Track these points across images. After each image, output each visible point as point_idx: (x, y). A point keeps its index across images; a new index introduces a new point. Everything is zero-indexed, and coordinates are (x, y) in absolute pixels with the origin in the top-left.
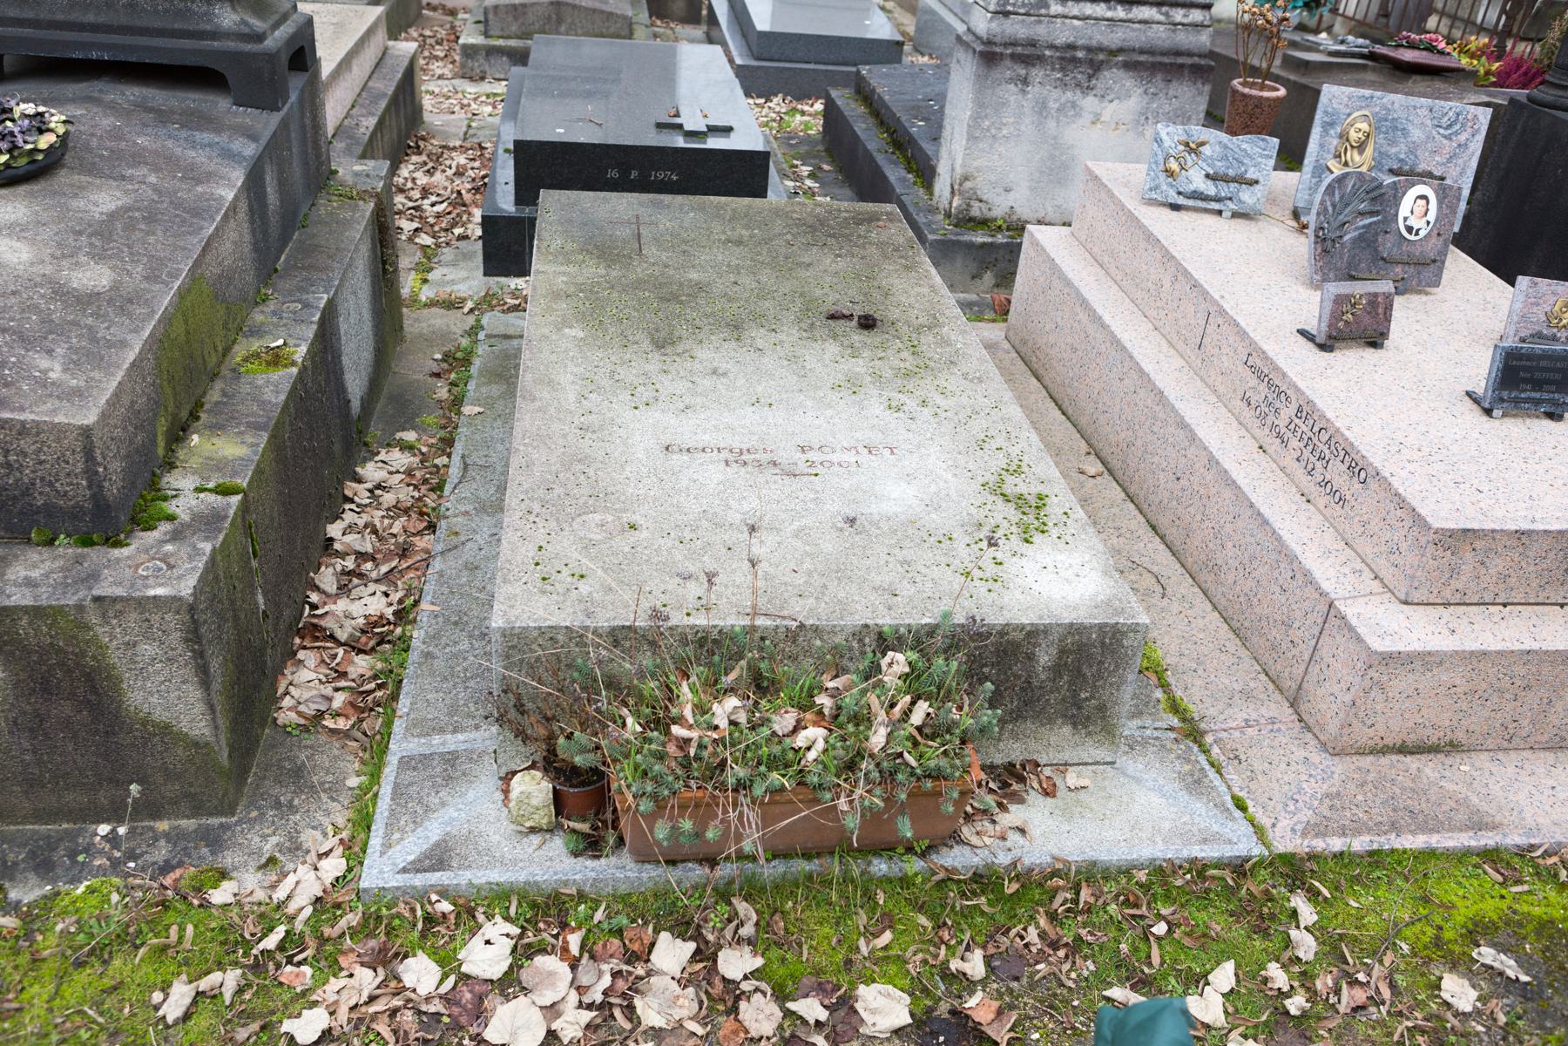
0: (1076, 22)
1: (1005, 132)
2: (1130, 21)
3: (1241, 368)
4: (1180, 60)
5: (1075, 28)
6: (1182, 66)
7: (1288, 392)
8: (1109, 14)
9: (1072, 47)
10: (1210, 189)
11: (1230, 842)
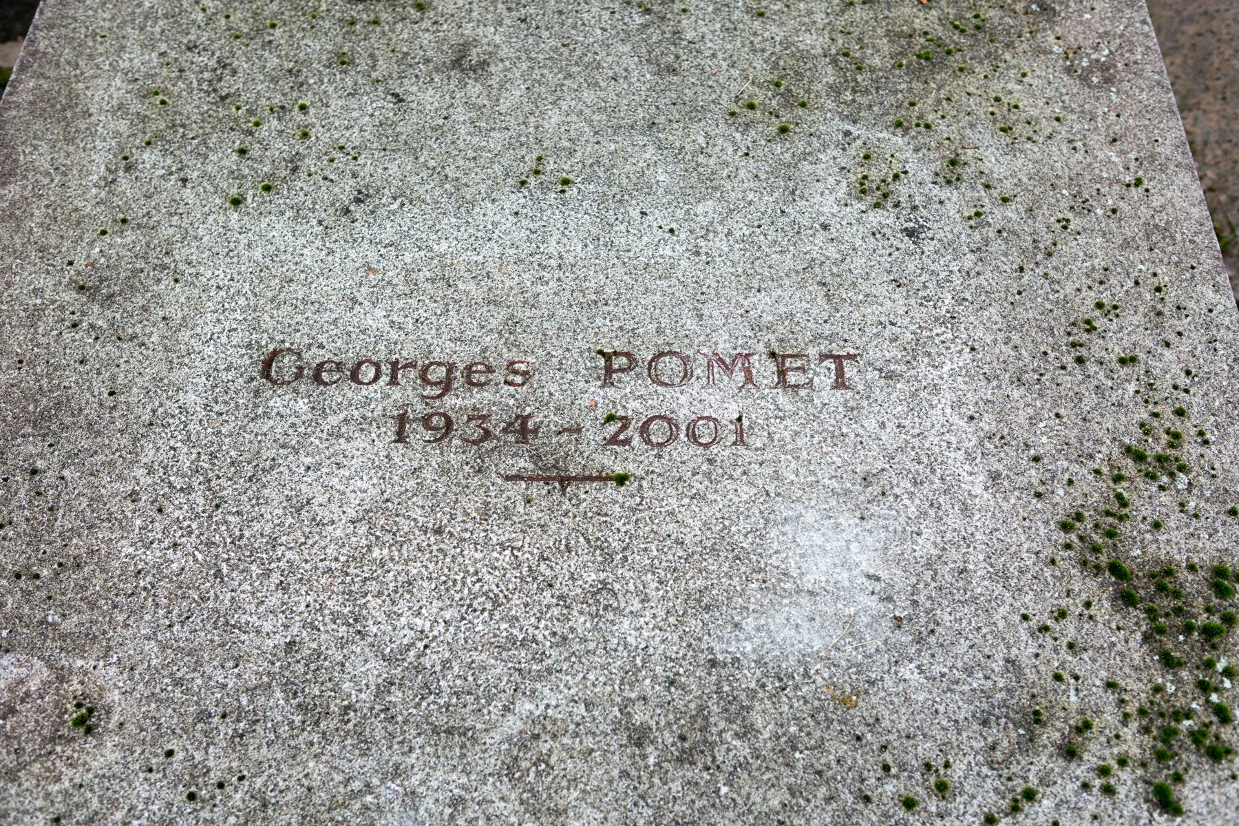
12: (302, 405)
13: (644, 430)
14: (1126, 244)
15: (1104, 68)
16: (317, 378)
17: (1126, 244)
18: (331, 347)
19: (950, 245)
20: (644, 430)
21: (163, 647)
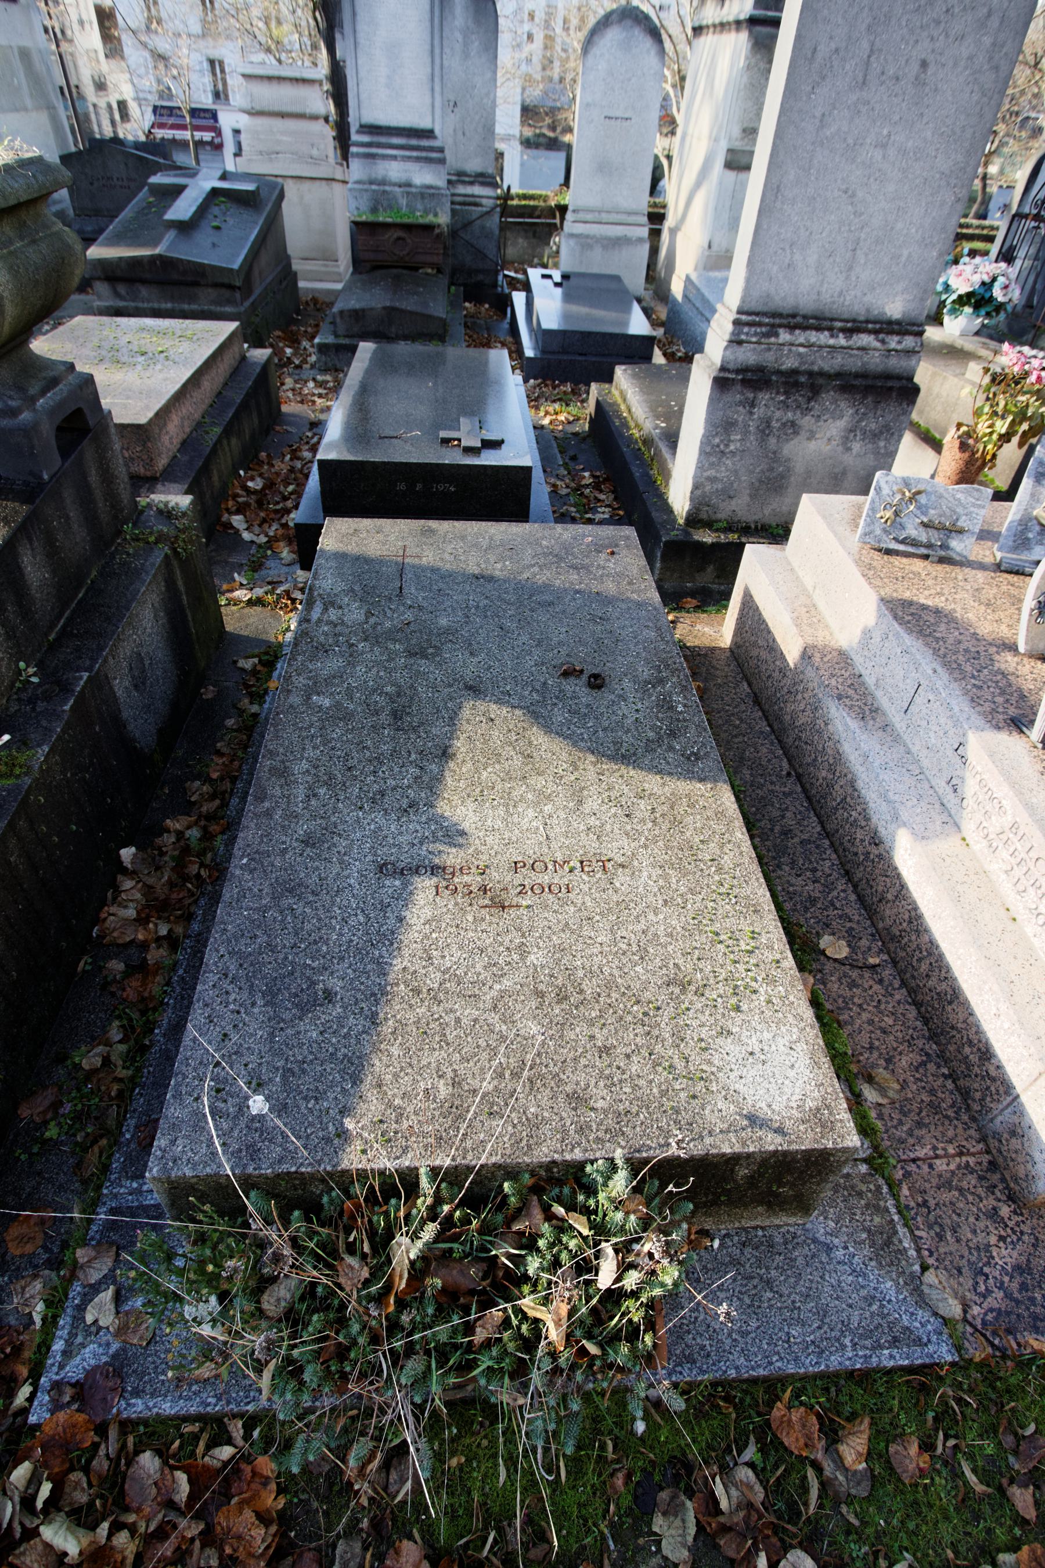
0: (801, 350)
1: (732, 447)
2: (849, 348)
3: (950, 752)
4: (890, 384)
5: (800, 354)
6: (891, 389)
7: (1004, 802)
8: (832, 342)
9: (794, 372)
10: (923, 536)
11: (919, 1342)
12: (397, 883)
13: (532, 889)
14: (708, 818)
15: (695, 754)
16: (402, 874)
17: (708, 818)
18: (405, 860)
19: (643, 821)
20: (532, 889)
21: (354, 971)
